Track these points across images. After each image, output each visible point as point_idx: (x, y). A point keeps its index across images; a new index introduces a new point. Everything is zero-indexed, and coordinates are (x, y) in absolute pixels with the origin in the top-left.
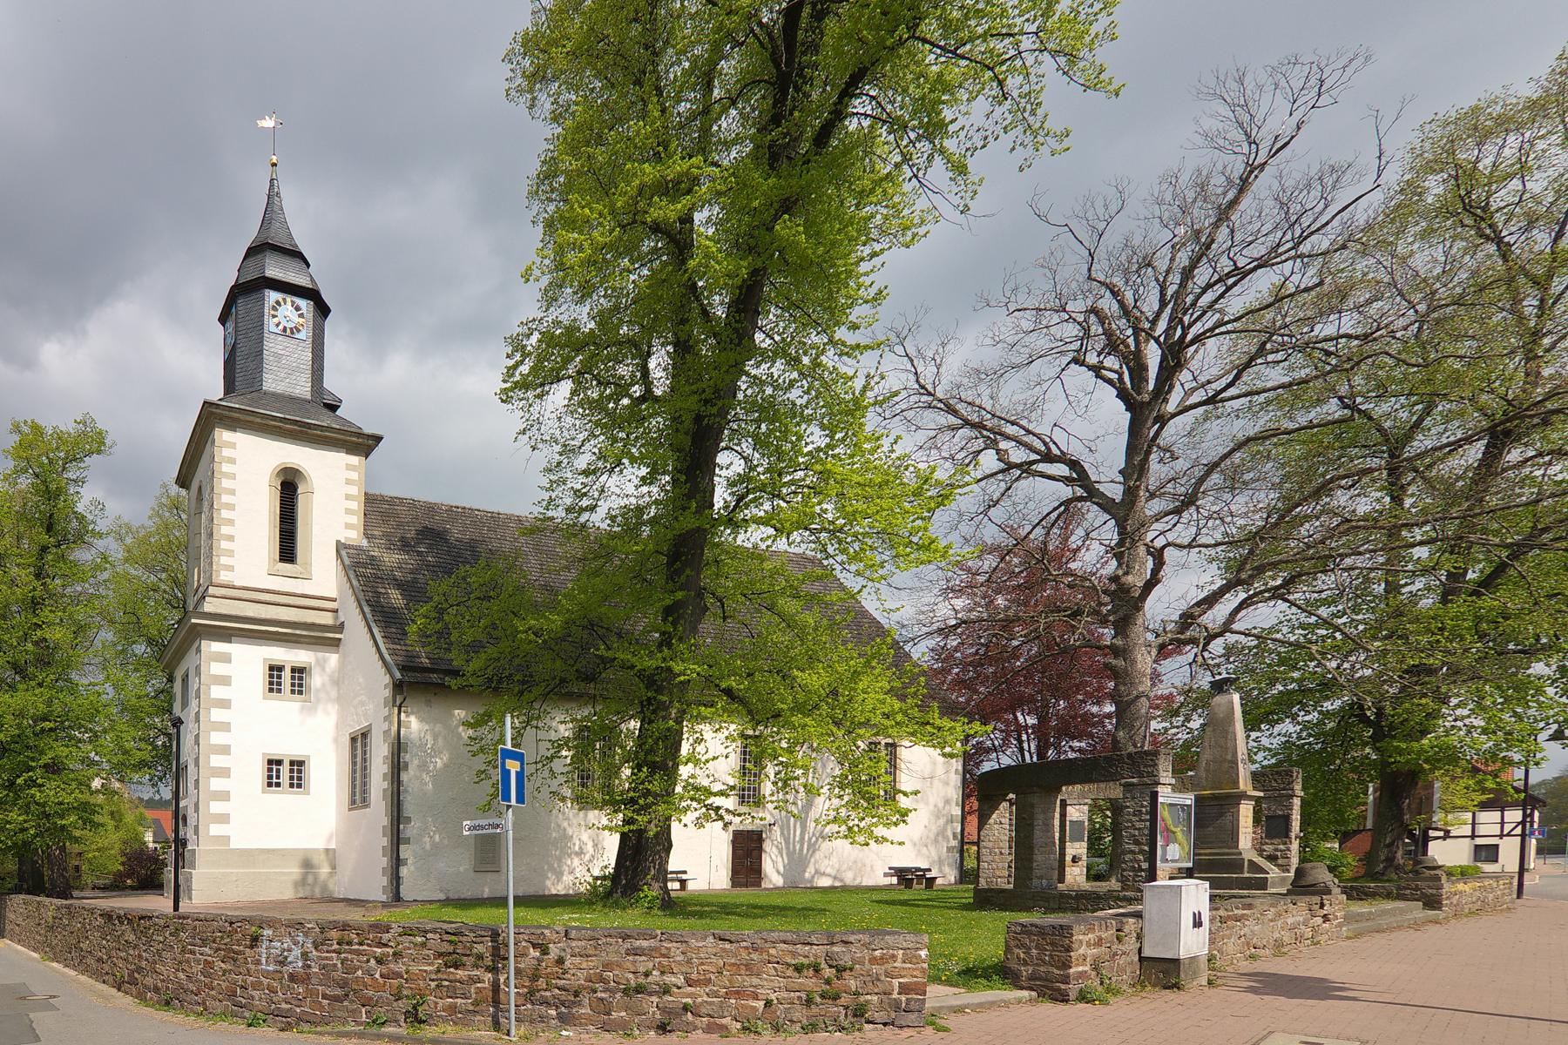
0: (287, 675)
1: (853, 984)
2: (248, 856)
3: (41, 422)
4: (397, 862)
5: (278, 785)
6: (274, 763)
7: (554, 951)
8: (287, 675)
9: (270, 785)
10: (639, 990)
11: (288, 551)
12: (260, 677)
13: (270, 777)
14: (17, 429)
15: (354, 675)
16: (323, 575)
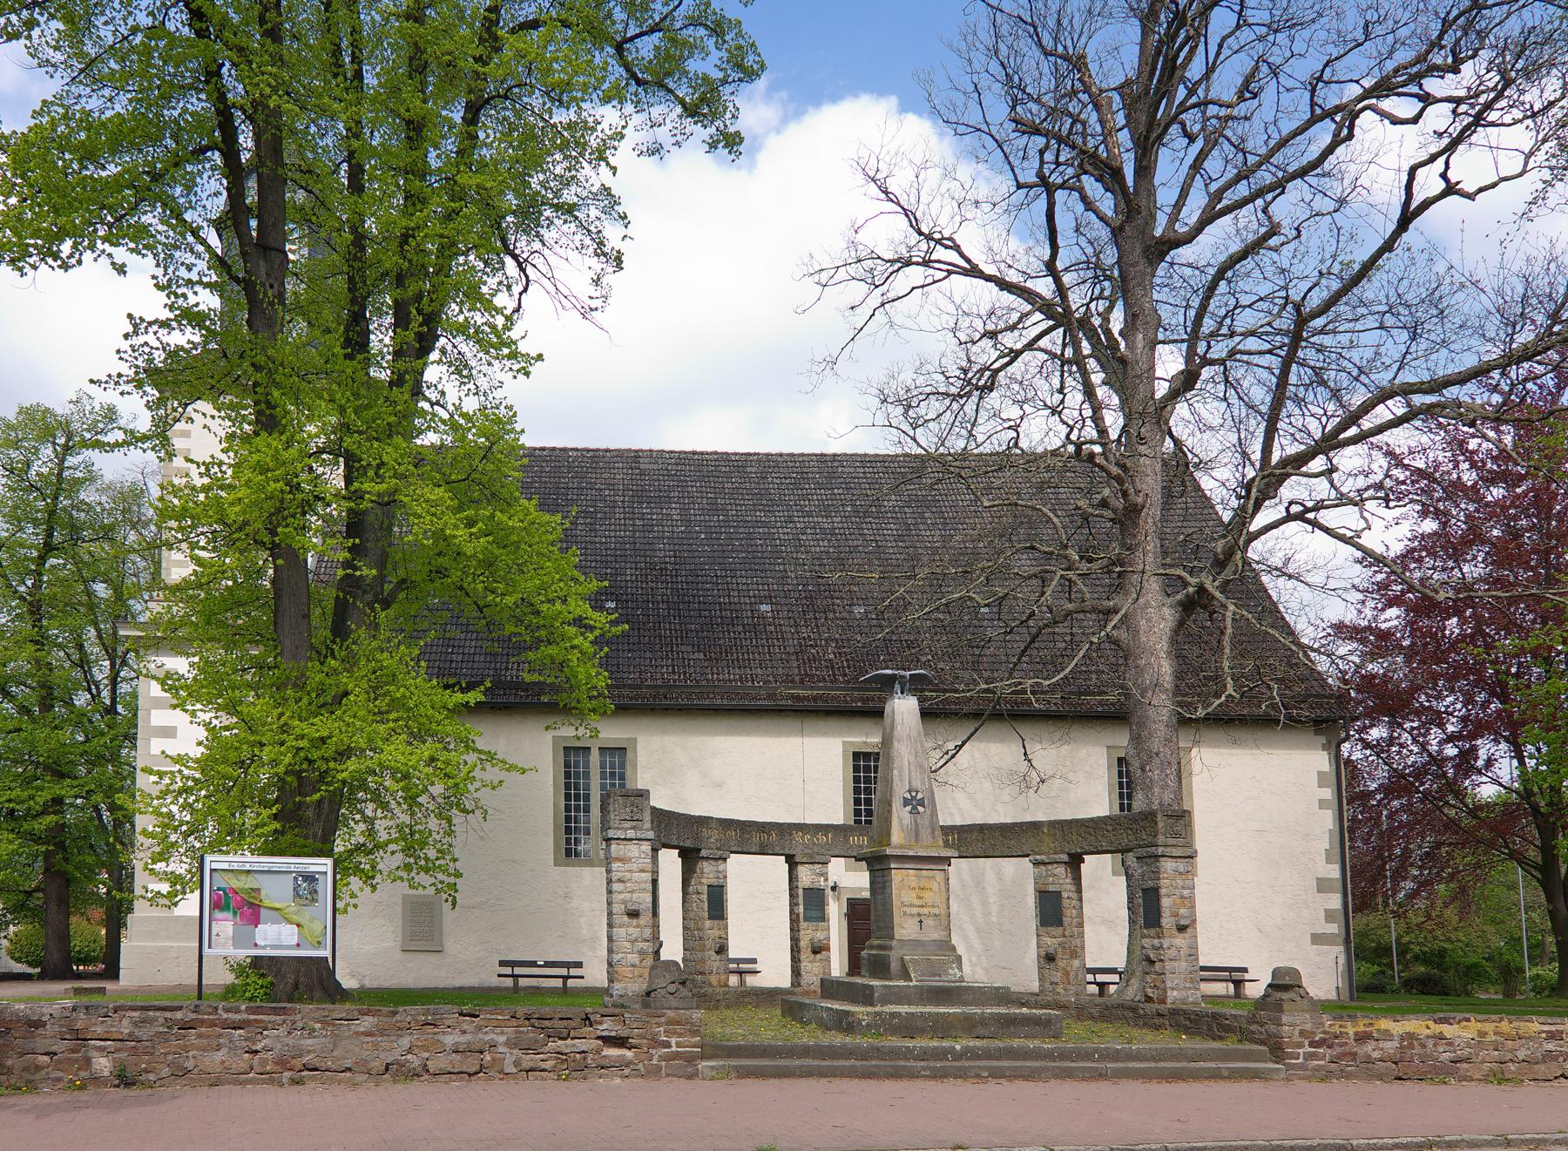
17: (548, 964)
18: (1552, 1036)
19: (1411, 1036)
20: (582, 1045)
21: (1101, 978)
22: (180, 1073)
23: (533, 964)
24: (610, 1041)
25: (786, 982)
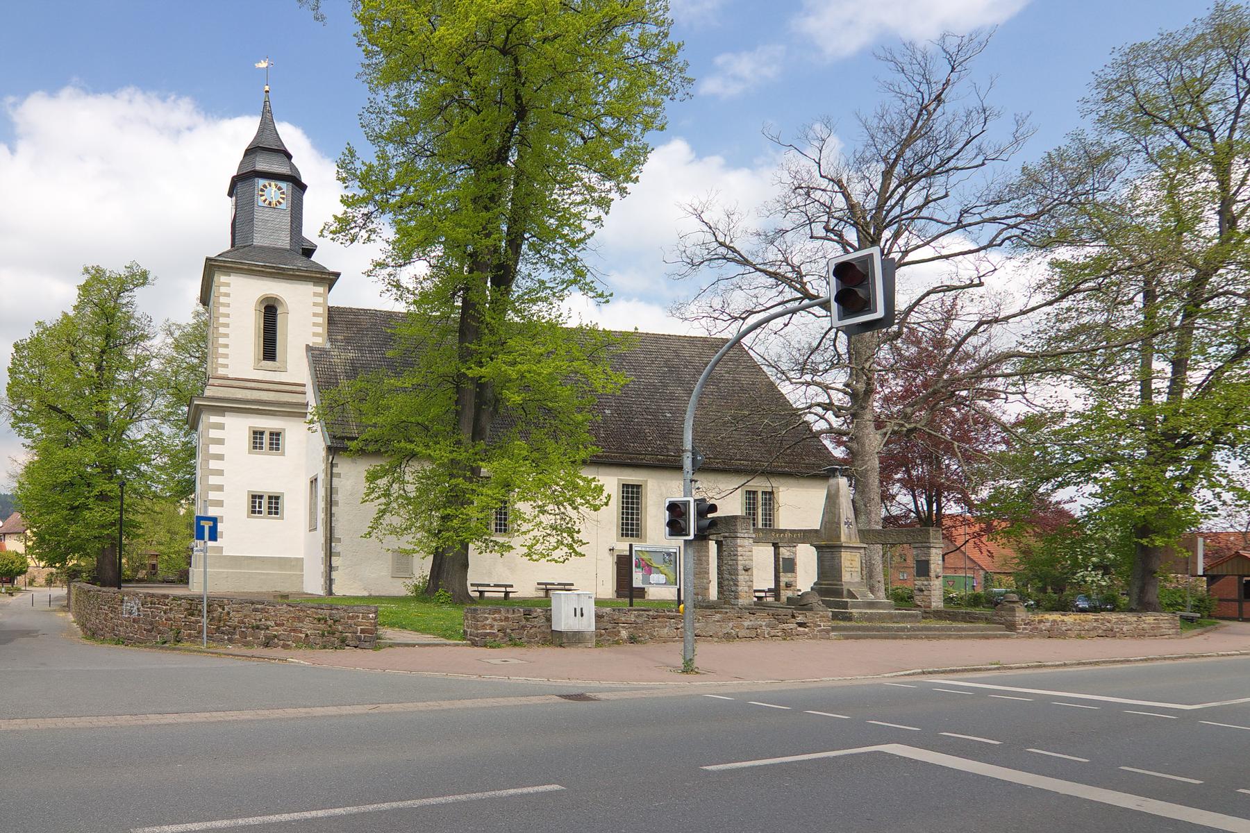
0: (266, 437)
1: (340, 628)
2: (236, 561)
3: (103, 266)
4: (330, 568)
5: (260, 512)
6: (256, 498)
7: (226, 609)
8: (266, 437)
9: (253, 512)
10: (258, 627)
11: (269, 350)
12: (245, 439)
13: (254, 507)
14: (87, 271)
15: (305, 443)
16: (295, 367)
17: (496, 586)
18: (1096, 620)
19: (1054, 621)
20: (791, 626)
21: (480, 589)
22: (652, 637)
23: (488, 585)
24: (800, 625)
25: (321, 592)
